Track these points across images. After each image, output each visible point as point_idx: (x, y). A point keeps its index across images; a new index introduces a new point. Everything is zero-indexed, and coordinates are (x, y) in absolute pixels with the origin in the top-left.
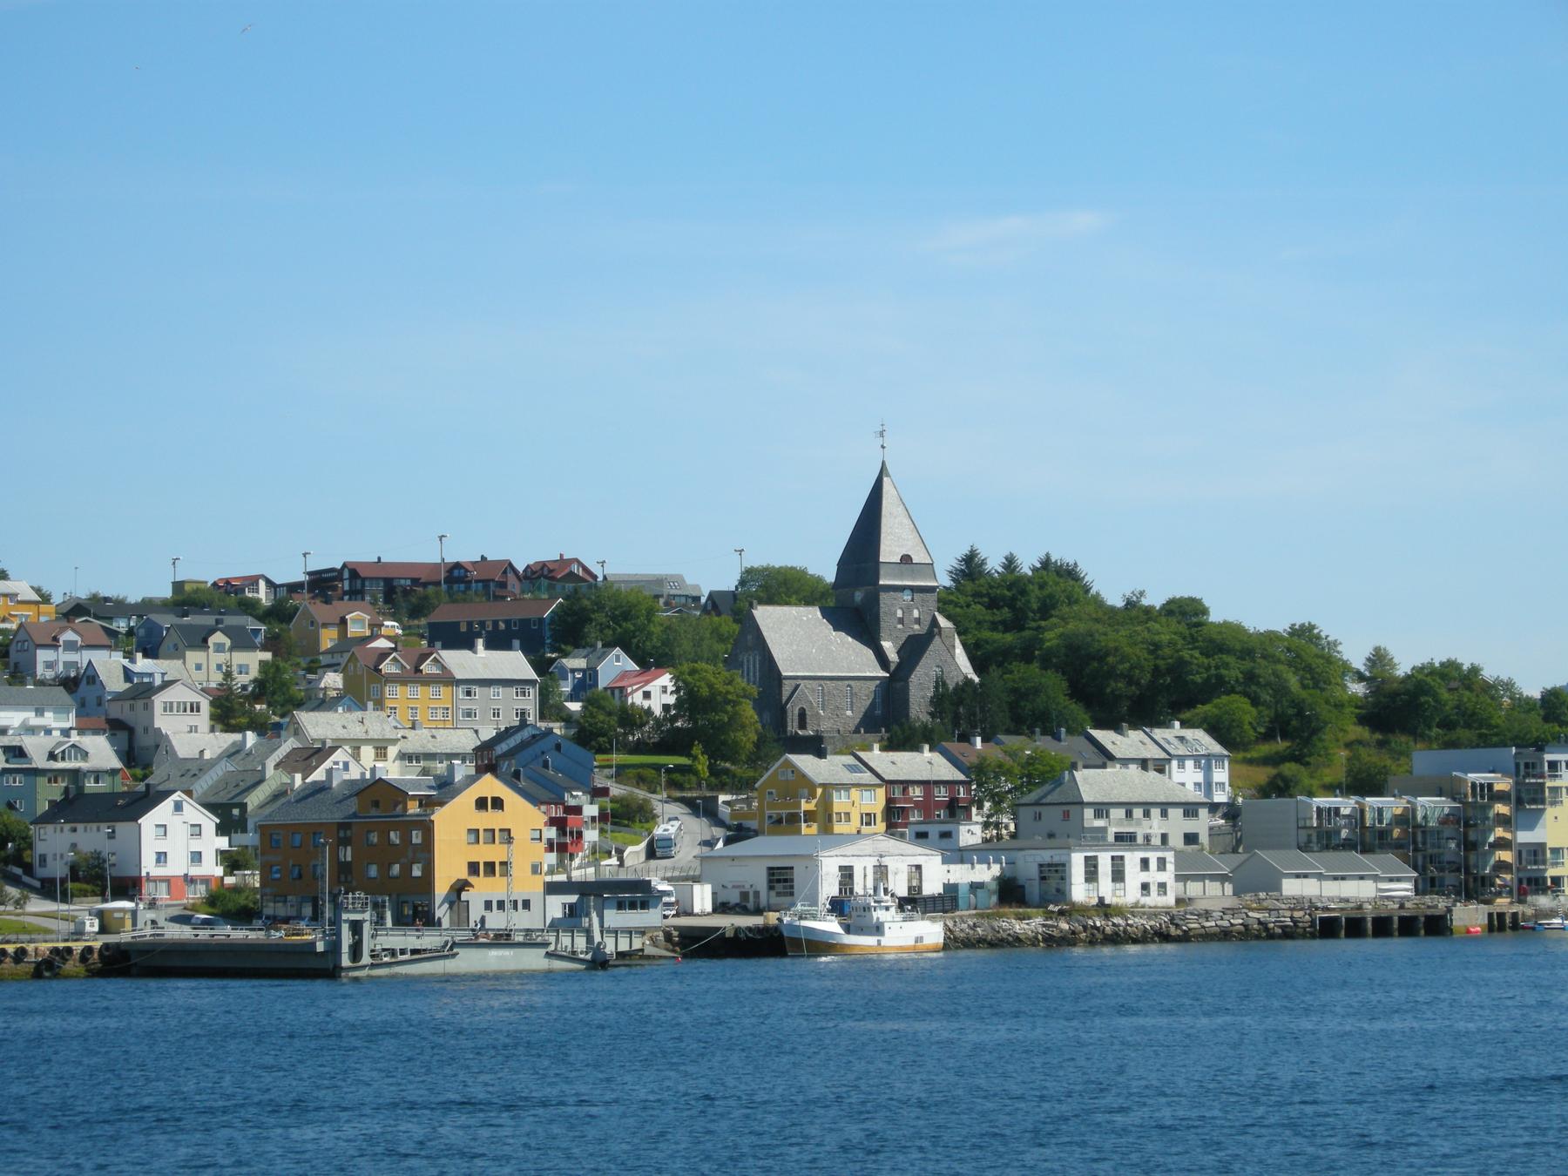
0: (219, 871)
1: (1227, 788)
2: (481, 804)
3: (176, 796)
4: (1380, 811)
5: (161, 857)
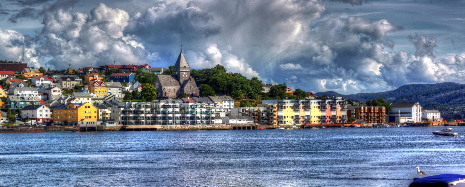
0: (51, 118)
1: (233, 106)
2: (86, 107)
3: (43, 106)
4: (253, 110)
5: (41, 115)
